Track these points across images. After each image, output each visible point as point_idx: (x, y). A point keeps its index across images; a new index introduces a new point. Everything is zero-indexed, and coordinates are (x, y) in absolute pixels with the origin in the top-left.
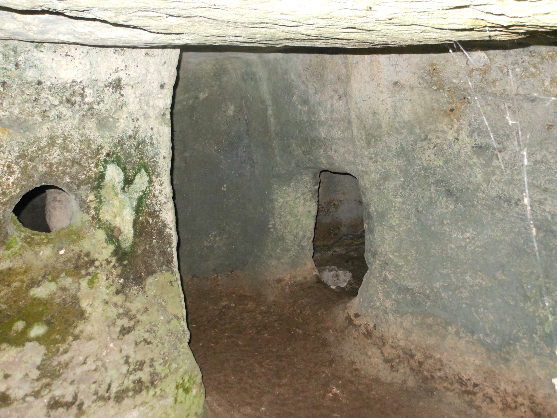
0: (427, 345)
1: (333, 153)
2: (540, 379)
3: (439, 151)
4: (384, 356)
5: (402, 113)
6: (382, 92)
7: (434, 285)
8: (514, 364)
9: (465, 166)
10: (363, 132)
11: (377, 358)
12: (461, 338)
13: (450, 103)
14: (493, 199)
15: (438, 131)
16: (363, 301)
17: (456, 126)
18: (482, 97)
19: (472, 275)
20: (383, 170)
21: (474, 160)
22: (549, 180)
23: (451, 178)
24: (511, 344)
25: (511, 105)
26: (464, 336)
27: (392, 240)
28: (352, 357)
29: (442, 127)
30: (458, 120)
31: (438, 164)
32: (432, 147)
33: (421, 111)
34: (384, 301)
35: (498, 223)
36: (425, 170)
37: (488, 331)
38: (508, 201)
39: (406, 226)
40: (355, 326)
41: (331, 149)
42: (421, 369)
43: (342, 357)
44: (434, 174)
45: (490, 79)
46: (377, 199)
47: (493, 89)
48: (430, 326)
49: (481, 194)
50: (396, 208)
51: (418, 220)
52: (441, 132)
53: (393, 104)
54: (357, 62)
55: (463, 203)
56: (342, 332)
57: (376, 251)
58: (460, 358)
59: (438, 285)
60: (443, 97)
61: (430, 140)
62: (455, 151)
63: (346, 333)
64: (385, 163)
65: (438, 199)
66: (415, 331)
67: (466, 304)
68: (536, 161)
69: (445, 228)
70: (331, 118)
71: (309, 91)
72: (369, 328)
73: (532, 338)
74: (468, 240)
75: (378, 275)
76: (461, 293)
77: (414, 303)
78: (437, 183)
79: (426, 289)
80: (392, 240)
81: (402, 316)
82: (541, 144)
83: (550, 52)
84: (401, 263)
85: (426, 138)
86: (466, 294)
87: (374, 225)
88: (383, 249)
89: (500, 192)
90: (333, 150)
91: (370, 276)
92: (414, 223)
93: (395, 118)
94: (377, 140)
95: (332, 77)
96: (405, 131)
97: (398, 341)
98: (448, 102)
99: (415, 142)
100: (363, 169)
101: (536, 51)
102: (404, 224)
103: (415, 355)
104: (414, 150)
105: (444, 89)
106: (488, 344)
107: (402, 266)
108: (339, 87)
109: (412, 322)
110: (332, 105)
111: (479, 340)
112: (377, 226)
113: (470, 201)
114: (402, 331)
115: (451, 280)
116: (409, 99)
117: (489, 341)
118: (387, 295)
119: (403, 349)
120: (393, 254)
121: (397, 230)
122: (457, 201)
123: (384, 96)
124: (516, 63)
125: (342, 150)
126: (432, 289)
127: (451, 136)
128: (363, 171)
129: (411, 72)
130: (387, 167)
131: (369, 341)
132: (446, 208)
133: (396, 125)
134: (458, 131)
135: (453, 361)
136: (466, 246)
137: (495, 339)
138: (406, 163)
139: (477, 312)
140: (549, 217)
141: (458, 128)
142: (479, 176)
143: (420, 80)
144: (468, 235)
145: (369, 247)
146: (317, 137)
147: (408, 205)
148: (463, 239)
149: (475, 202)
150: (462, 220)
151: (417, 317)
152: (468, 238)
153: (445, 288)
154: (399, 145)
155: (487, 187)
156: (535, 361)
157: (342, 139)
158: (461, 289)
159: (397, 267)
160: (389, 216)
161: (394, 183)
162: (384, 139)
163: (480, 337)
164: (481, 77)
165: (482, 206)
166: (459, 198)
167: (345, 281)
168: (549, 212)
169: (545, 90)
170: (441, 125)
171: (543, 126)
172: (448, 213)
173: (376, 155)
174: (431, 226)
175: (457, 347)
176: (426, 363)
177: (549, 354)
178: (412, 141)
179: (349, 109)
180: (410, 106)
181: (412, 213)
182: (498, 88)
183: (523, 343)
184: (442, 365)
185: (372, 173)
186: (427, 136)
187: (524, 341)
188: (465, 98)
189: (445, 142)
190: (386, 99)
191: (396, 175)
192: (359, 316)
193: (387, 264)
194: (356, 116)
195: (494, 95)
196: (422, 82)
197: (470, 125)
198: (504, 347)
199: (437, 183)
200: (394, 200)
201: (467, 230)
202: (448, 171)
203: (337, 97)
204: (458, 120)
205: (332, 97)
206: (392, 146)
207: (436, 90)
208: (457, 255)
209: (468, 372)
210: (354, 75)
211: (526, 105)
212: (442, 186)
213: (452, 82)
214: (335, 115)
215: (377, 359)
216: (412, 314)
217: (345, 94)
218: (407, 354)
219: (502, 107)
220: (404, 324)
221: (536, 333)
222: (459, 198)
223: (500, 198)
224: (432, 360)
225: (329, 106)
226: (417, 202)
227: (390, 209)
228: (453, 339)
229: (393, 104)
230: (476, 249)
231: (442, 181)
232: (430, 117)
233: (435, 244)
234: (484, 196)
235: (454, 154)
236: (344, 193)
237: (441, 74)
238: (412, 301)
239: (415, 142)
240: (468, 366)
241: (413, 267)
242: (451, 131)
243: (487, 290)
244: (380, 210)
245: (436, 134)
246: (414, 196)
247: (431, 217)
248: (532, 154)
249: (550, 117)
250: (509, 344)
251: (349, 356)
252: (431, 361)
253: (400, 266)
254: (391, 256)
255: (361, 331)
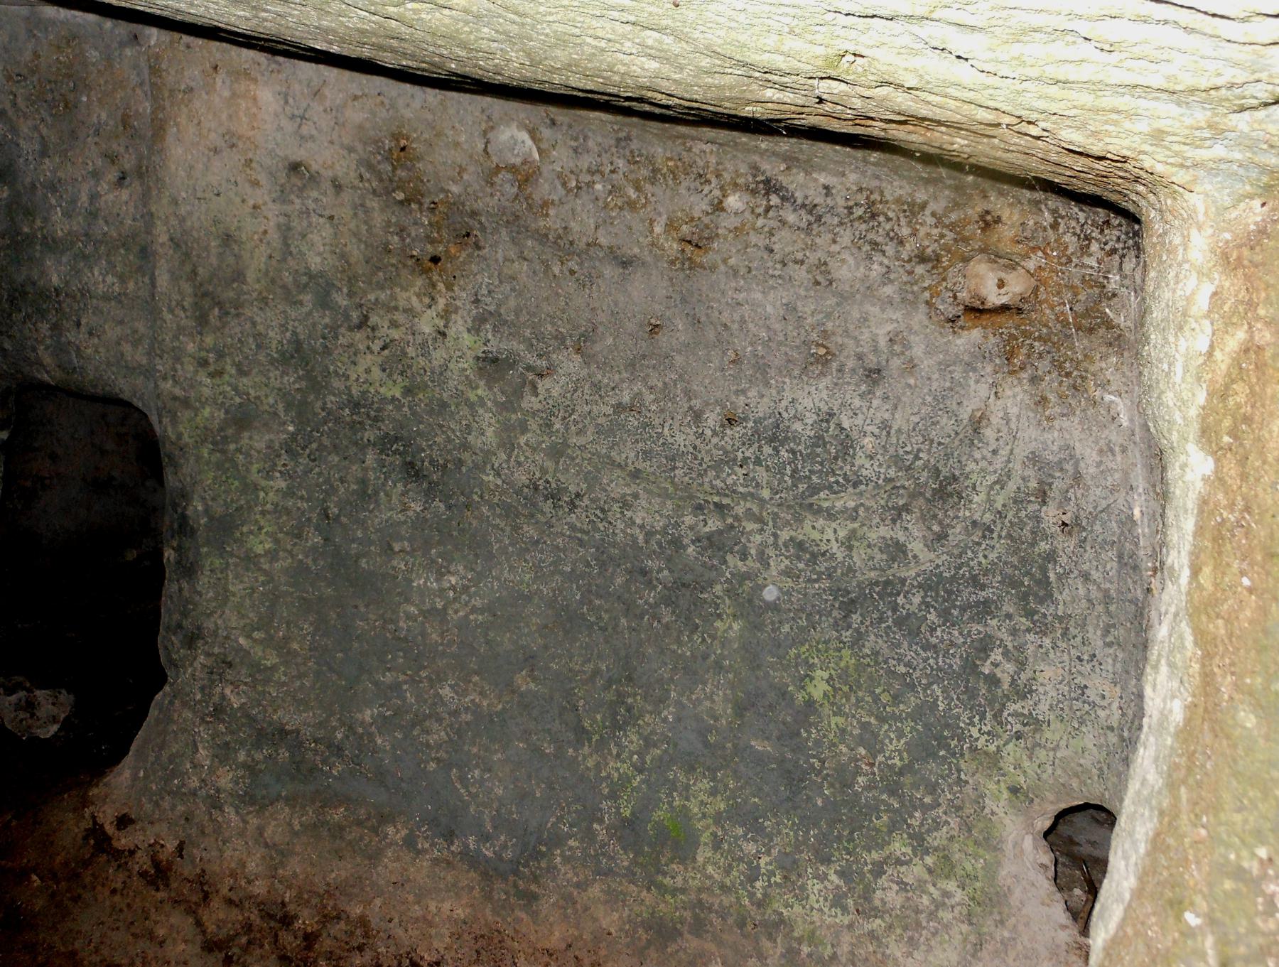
0: (328, 884)
1: (83, 336)
2: (610, 934)
3: (395, 360)
4: (204, 932)
5: (304, 249)
6: (255, 184)
7: (359, 716)
8: (545, 906)
9: (457, 405)
10: (187, 288)
11: (186, 941)
12: (419, 852)
13: (432, 241)
14: (518, 492)
15: (396, 308)
16: (146, 777)
17: (442, 302)
18: (513, 240)
19: (456, 684)
20: (238, 400)
21: (480, 392)
22: (645, 452)
23: (419, 433)
24: (543, 855)
25: (576, 268)
26: (427, 846)
27: (251, 595)
28: (105, 952)
29: (408, 299)
30: (449, 287)
31: (389, 395)
32: (376, 348)
33: (356, 252)
34: (212, 770)
35: (527, 550)
36: (356, 406)
37: (489, 828)
38: (554, 496)
39: (292, 556)
40: (117, 854)
41: (78, 324)
42: (312, 954)
43: (74, 953)
44: (376, 419)
45: (536, 197)
46: (215, 478)
47: (542, 224)
48: (338, 831)
49: (491, 478)
50: (269, 507)
51: (326, 540)
52: (405, 311)
53: (282, 220)
54: (191, 90)
55: (446, 498)
56: (75, 876)
57: (199, 628)
58: (416, 907)
59: (367, 715)
60: (415, 224)
61: (373, 329)
62: (435, 363)
63: (88, 880)
64: (245, 380)
65: (383, 485)
66: (298, 849)
67: (438, 760)
68: (619, 405)
69: (395, 563)
70: (86, 235)
71: (22, 142)
72: (163, 857)
73: (590, 835)
74: (451, 594)
75: (198, 697)
76: (428, 732)
77: (298, 770)
78: (384, 444)
79: (335, 729)
80: (251, 595)
81: (263, 808)
82: (633, 365)
83: (671, 159)
84: (272, 659)
85: (363, 323)
86: (438, 734)
87: (198, 553)
88: (219, 622)
89: (538, 475)
90: (83, 329)
91: (171, 703)
92: (314, 548)
93: (284, 260)
94: (227, 313)
95: (104, 116)
96: (307, 298)
97: (249, 882)
98: (428, 237)
99: (334, 329)
100: (178, 391)
101: (644, 152)
102: (286, 550)
103: (296, 917)
104: (327, 351)
105: (421, 204)
106: (487, 860)
107: (273, 668)
108: (122, 150)
109: (290, 824)
110: (94, 197)
111: (465, 853)
112: (208, 554)
113: (462, 494)
114: (260, 852)
115: (404, 699)
116: (327, 213)
117: (489, 854)
118: (223, 753)
119: (260, 905)
120: (249, 637)
121: (266, 567)
122: (429, 494)
123: (260, 196)
124: (598, 171)
125: (112, 332)
126: (351, 728)
127: (427, 324)
128: (175, 398)
129: (342, 146)
130: (252, 392)
131: (161, 895)
132: (402, 511)
133: (287, 278)
134: (446, 314)
135: (396, 920)
136: (445, 608)
137: (505, 847)
138: (304, 384)
139: (463, 779)
140: (641, 538)
141: (446, 305)
142: (490, 432)
143: (363, 170)
144: (453, 580)
145: (176, 616)
146: (34, 284)
147: (302, 498)
148: (439, 590)
149: (476, 498)
150: (439, 543)
151: (303, 807)
152: (453, 588)
153: (384, 723)
154: (288, 334)
155: (508, 461)
156: (595, 891)
157: (118, 298)
158: (427, 723)
159: (259, 671)
160: (245, 529)
161: (267, 437)
162: (247, 312)
163: (467, 846)
164: (515, 190)
165: (492, 507)
166: (437, 484)
167: (54, 719)
168: (642, 527)
169: (653, 244)
170: (405, 295)
171: (641, 326)
172: (405, 522)
173: (221, 355)
174: (358, 556)
175: (409, 880)
176: (325, 935)
177: (627, 868)
178: (326, 326)
179: (152, 215)
180: (327, 231)
181: (309, 519)
182: (552, 221)
183: (571, 848)
184: (366, 935)
185: (203, 405)
186: (366, 318)
187: (572, 843)
188: (468, 235)
189: (410, 337)
190: (265, 204)
191: (275, 414)
192: (132, 821)
193: (230, 665)
194: (171, 239)
195: (542, 237)
196: (367, 175)
197: (477, 301)
198: (526, 865)
199: (384, 444)
200: (263, 483)
201: (452, 569)
202: (414, 413)
203: (112, 175)
204: (449, 287)
205: (96, 175)
206: (271, 334)
207: (401, 202)
208: (424, 634)
209: (436, 944)
210: (177, 125)
211: (609, 271)
212: (394, 453)
213: (443, 190)
214: (101, 227)
215: (183, 946)
216: (291, 801)
217: (141, 173)
218: (271, 917)
219: (556, 270)
220: (268, 833)
221: (601, 821)
222: (437, 484)
223: (536, 488)
224: (342, 925)
225: (84, 198)
226: (326, 491)
227: (250, 508)
228: (398, 859)
229: (282, 220)
230: (471, 617)
231: (397, 439)
232: (379, 269)
233: (367, 606)
234: (499, 482)
235: (433, 372)
236: (54, 457)
237: (420, 165)
238: (293, 766)
239: (334, 329)
240: (437, 927)
241: (302, 669)
242: (429, 311)
243: (492, 721)
244: (219, 510)
245: (389, 316)
246: (320, 474)
247: (359, 534)
248: (613, 389)
249: (656, 306)
250: (538, 855)
251: (97, 951)
252: (339, 928)
253: (267, 668)
254: (242, 641)
255: (137, 868)
